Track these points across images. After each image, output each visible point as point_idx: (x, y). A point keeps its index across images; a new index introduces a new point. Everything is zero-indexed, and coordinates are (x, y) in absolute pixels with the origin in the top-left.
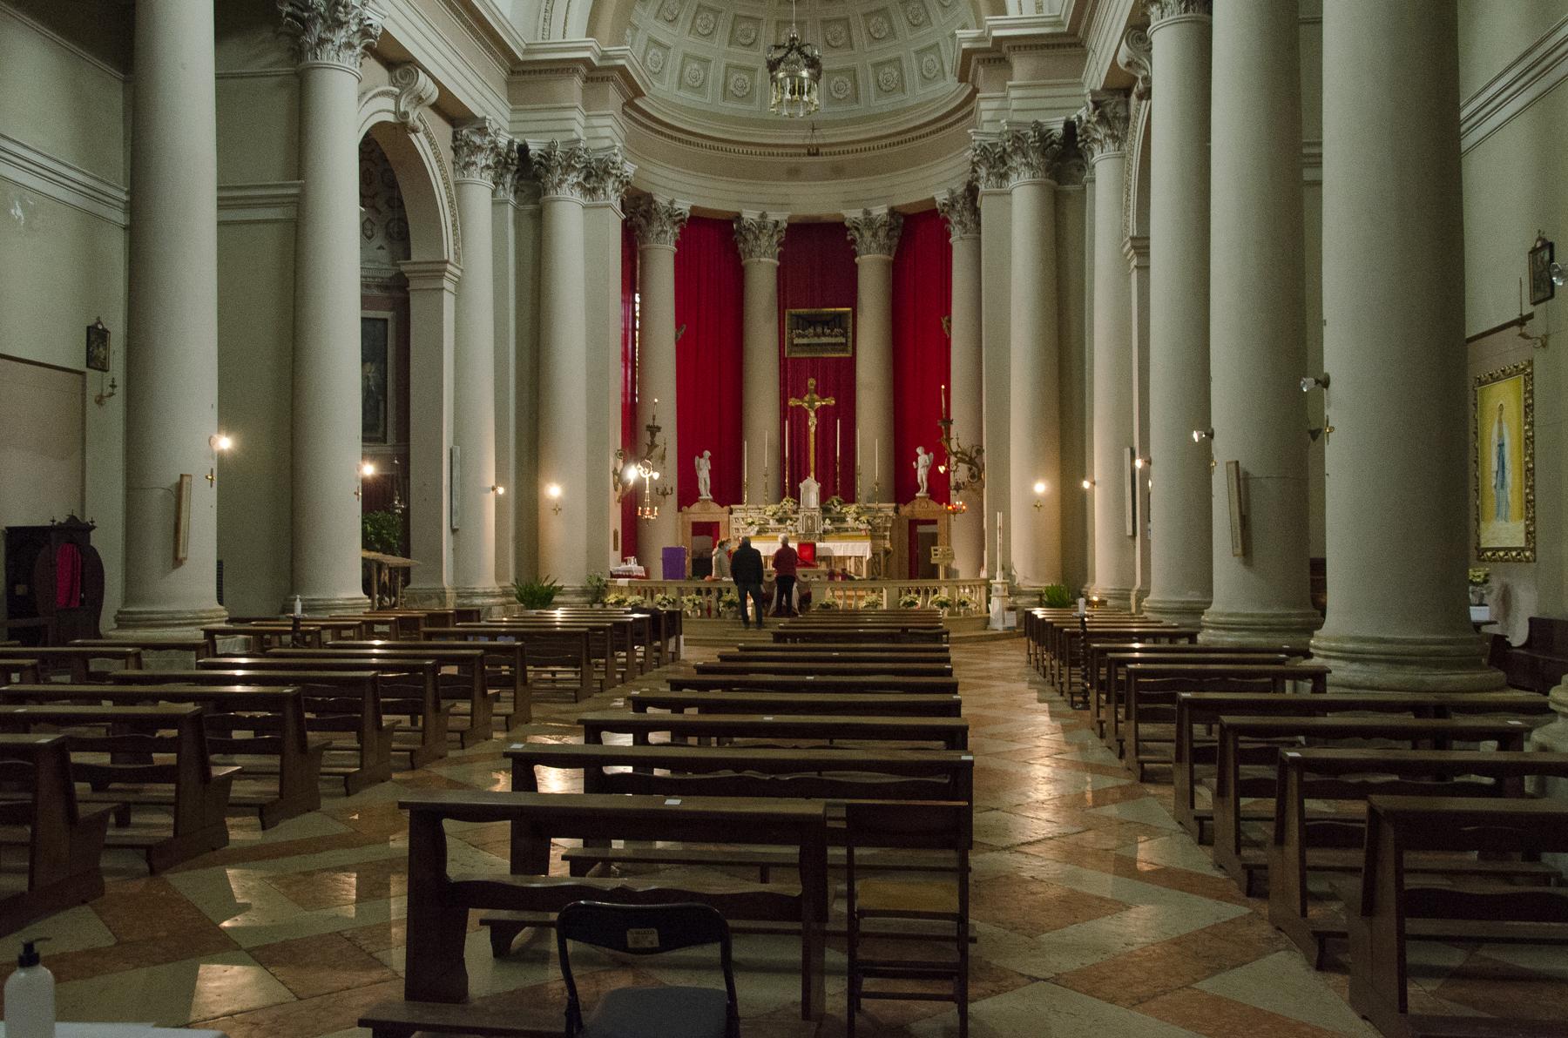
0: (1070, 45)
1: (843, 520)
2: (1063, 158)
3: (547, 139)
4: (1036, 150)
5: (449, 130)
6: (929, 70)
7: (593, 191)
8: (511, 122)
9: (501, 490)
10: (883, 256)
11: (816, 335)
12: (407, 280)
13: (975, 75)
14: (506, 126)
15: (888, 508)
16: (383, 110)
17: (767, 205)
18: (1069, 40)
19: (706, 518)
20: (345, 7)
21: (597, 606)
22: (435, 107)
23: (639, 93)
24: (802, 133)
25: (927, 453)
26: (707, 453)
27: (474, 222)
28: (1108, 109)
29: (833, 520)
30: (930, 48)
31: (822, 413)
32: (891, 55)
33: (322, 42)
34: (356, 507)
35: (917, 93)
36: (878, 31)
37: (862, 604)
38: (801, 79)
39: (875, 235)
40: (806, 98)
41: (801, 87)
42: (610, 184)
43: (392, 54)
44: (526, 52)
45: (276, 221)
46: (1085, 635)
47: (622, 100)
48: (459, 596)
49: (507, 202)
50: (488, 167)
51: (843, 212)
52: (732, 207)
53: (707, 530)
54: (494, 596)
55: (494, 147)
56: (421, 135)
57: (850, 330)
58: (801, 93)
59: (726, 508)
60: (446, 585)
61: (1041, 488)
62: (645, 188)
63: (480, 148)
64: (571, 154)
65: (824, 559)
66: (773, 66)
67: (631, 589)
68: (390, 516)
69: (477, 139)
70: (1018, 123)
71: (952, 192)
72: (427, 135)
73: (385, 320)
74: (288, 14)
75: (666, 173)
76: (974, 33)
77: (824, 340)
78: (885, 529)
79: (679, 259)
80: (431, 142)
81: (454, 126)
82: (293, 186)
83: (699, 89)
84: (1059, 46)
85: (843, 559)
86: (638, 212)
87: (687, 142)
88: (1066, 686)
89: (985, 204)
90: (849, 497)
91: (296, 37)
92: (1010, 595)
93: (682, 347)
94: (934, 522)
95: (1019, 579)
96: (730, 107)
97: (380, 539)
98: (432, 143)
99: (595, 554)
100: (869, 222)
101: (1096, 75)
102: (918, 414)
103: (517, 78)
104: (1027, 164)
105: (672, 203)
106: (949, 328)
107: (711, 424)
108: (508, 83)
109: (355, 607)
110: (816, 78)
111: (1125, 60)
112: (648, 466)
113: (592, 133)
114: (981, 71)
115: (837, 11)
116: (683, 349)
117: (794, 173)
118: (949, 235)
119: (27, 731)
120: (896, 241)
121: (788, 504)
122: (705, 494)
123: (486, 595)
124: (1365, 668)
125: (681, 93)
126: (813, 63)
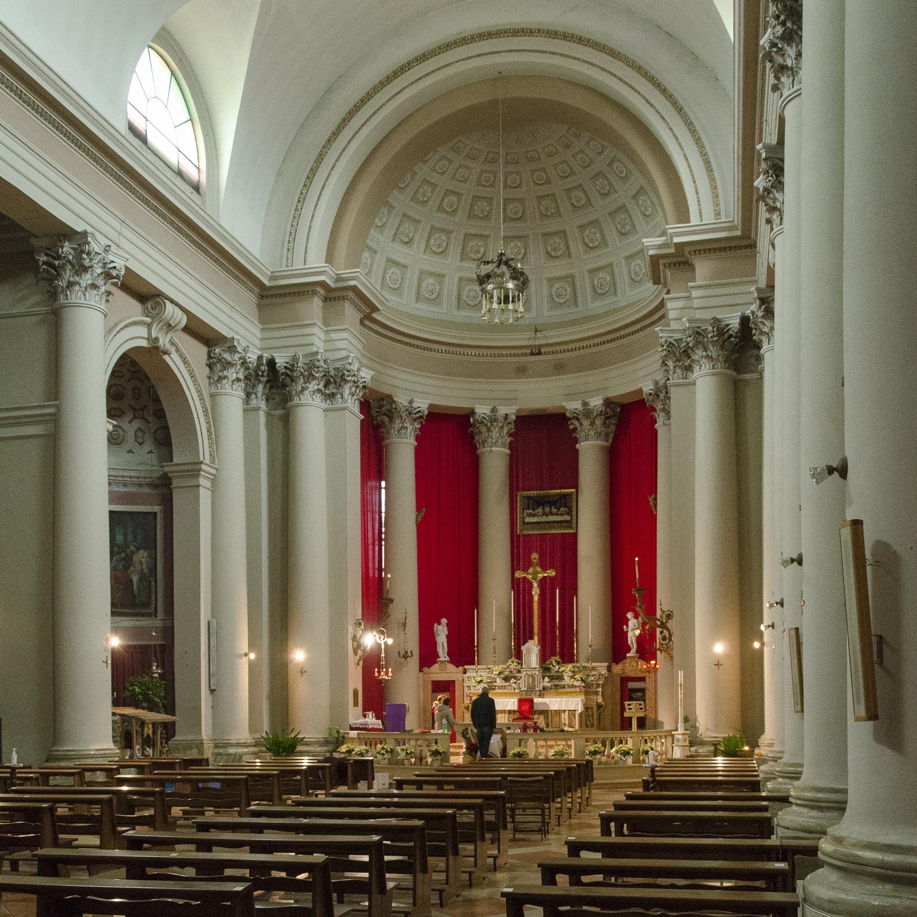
1: (561, 678)
3: (290, 353)
4: (714, 343)
5: (204, 349)
6: (636, 274)
7: (332, 396)
8: (262, 339)
9: (252, 656)
10: (599, 442)
12: (170, 479)
13: (665, 278)
14: (258, 343)
15: (602, 667)
16: (135, 337)
17: (496, 401)
18: (743, 243)
19: (443, 677)
20: (89, 254)
22: (186, 329)
23: (375, 309)
24: (527, 335)
26: (444, 621)
27: (226, 430)
29: (552, 678)
31: (543, 582)
32: (605, 262)
33: (71, 285)
34: (106, 674)
37: (551, 752)
38: (507, 290)
39: (592, 424)
41: (506, 298)
42: (347, 389)
43: (144, 290)
44: (272, 278)
45: (41, 436)
47: (359, 316)
48: (216, 746)
49: (258, 409)
51: (564, 404)
52: (464, 404)
53: (444, 687)
55: (244, 363)
56: (174, 355)
59: (461, 668)
60: (204, 736)
61: (719, 648)
62: (386, 390)
63: (230, 364)
64: (311, 366)
65: (541, 712)
66: (483, 280)
67: (360, 739)
68: (149, 677)
69: (227, 356)
71: (656, 383)
73: (155, 514)
74: (44, 263)
75: (405, 376)
76: (660, 240)
77: (552, 518)
78: (598, 685)
80: (185, 362)
81: (209, 347)
82: (49, 406)
83: (436, 300)
84: (730, 248)
85: (558, 713)
90: (568, 656)
91: (51, 279)
92: (692, 744)
93: (422, 529)
94: (643, 679)
95: (702, 730)
97: (147, 699)
98: (185, 361)
99: (337, 710)
100: (587, 412)
102: (632, 582)
103: (265, 301)
104: (707, 357)
105: (411, 402)
106: (656, 505)
107: (450, 593)
108: (260, 307)
109: (103, 756)
112: (382, 633)
113: (330, 346)
114: (668, 273)
115: (553, 226)
117: (521, 371)
119: (210, 851)
121: (513, 664)
124: (820, 814)
125: (419, 306)
126: (516, 275)
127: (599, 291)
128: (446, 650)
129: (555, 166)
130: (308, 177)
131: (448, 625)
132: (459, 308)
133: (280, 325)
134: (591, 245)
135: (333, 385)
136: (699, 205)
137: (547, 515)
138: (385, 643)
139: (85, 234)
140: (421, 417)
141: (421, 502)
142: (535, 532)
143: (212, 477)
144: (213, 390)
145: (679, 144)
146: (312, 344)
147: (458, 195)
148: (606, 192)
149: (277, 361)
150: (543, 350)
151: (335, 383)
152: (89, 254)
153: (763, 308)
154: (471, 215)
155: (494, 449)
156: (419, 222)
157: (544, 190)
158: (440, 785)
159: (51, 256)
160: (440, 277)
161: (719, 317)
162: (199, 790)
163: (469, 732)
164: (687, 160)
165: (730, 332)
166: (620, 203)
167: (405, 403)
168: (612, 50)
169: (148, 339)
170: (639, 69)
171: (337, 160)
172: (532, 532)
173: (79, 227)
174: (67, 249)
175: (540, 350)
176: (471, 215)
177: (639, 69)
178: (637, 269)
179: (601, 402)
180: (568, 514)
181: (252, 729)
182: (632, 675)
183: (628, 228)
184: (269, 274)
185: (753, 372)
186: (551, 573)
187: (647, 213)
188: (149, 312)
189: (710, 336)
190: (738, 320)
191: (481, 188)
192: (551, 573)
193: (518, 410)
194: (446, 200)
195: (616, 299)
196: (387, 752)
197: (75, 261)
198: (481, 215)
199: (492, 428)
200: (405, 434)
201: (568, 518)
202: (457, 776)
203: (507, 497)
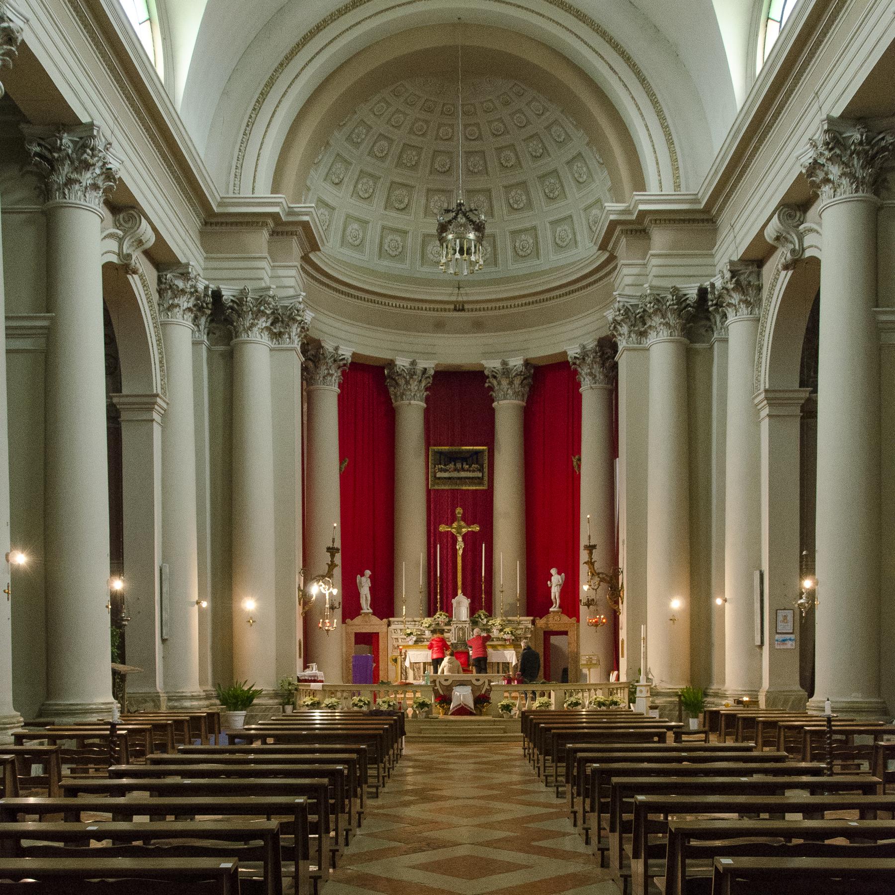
0: (703, 221)
2: (697, 319)
7: (280, 335)
8: (204, 269)
11: (456, 470)
15: (526, 621)
18: (705, 217)
20: (93, 149)
21: (289, 709)
22: (146, 253)
23: (315, 247)
24: (449, 290)
25: (559, 573)
26: (368, 573)
28: (742, 278)
30: (565, 219)
32: (528, 225)
33: (70, 182)
35: (550, 259)
36: (516, 202)
39: (511, 383)
40: (473, 258)
41: (469, 249)
42: (295, 330)
44: (220, 205)
46: (614, 731)
48: (170, 699)
49: (201, 343)
50: (189, 309)
51: (483, 362)
52: (386, 355)
54: (201, 699)
57: (486, 465)
58: (469, 253)
59: (385, 620)
61: (719, 601)
66: (443, 228)
69: (180, 284)
70: (659, 288)
72: (142, 277)
76: (621, 206)
77: (463, 474)
79: (342, 400)
80: (143, 283)
81: (158, 269)
82: (44, 318)
83: (359, 247)
86: (312, 353)
87: (348, 295)
88: (542, 769)
89: (623, 361)
93: (344, 478)
94: (565, 633)
95: (656, 682)
96: (385, 265)
99: (282, 659)
101: (733, 244)
102: (551, 537)
104: (667, 324)
106: (579, 466)
107: (367, 548)
108: (202, 234)
110: (479, 240)
111: (774, 236)
114: (623, 241)
116: (346, 480)
117: (439, 326)
118: (579, 385)
120: (527, 389)
122: (366, 607)
123: (192, 698)
126: (479, 228)
127: (521, 253)
128: (369, 602)
129: (490, 122)
130: (258, 101)
131: (370, 577)
132: (380, 257)
133: (236, 256)
134: (515, 206)
135: (280, 324)
136: (659, 175)
137: (458, 471)
138: (331, 594)
139: (91, 126)
140: (345, 365)
141: (344, 451)
142: (446, 488)
143: (163, 412)
144: (163, 319)
145: (641, 114)
146: (262, 279)
147: (391, 141)
148: (538, 154)
149: (223, 293)
150: (466, 306)
151: (282, 322)
152: (93, 149)
153: (734, 280)
154: (399, 164)
155: (412, 402)
156: (351, 164)
157: (476, 146)
158: (263, 739)
159: (46, 148)
160: (364, 223)
161: (678, 286)
162: (84, 746)
163: (438, 684)
164: (648, 130)
165: (688, 302)
166: (552, 168)
167: (331, 349)
168: (578, 11)
169: (119, 255)
170: (604, 34)
171: (289, 87)
172: (443, 487)
173: (85, 119)
174: (66, 140)
175: (463, 306)
176: (399, 164)
177: (604, 34)
178: (562, 234)
179: (522, 362)
180: (479, 470)
181: (201, 683)
182: (555, 628)
183: (557, 193)
184: (219, 199)
185: (704, 342)
186: (476, 528)
187: (581, 180)
188: (121, 225)
189: (668, 304)
190: (696, 291)
191: (413, 137)
192: (476, 528)
193: (437, 365)
194: (378, 144)
195: (538, 262)
196: (365, 704)
197: (74, 156)
198: (409, 165)
199: (411, 382)
200: (331, 381)
201: (480, 475)
202: (86, 730)
203: (423, 452)
